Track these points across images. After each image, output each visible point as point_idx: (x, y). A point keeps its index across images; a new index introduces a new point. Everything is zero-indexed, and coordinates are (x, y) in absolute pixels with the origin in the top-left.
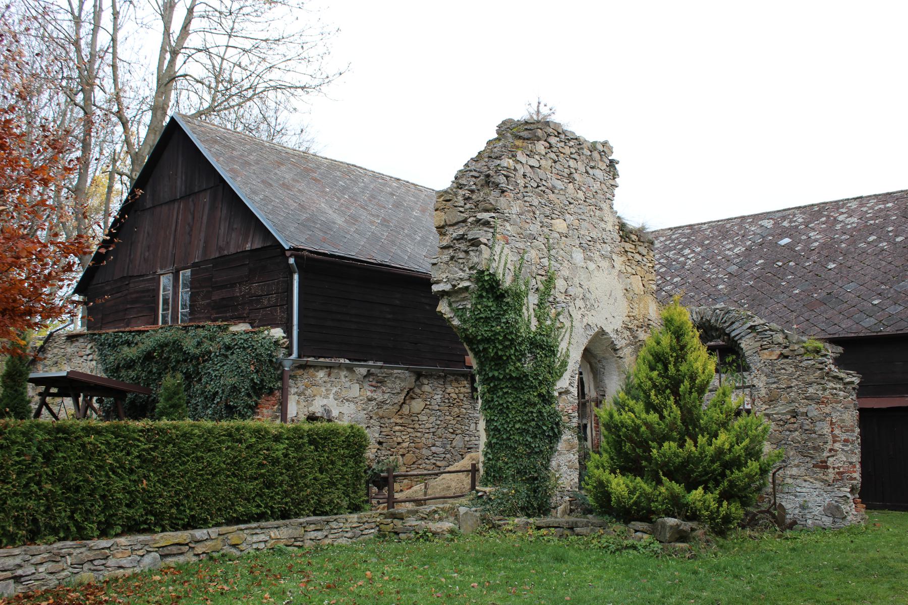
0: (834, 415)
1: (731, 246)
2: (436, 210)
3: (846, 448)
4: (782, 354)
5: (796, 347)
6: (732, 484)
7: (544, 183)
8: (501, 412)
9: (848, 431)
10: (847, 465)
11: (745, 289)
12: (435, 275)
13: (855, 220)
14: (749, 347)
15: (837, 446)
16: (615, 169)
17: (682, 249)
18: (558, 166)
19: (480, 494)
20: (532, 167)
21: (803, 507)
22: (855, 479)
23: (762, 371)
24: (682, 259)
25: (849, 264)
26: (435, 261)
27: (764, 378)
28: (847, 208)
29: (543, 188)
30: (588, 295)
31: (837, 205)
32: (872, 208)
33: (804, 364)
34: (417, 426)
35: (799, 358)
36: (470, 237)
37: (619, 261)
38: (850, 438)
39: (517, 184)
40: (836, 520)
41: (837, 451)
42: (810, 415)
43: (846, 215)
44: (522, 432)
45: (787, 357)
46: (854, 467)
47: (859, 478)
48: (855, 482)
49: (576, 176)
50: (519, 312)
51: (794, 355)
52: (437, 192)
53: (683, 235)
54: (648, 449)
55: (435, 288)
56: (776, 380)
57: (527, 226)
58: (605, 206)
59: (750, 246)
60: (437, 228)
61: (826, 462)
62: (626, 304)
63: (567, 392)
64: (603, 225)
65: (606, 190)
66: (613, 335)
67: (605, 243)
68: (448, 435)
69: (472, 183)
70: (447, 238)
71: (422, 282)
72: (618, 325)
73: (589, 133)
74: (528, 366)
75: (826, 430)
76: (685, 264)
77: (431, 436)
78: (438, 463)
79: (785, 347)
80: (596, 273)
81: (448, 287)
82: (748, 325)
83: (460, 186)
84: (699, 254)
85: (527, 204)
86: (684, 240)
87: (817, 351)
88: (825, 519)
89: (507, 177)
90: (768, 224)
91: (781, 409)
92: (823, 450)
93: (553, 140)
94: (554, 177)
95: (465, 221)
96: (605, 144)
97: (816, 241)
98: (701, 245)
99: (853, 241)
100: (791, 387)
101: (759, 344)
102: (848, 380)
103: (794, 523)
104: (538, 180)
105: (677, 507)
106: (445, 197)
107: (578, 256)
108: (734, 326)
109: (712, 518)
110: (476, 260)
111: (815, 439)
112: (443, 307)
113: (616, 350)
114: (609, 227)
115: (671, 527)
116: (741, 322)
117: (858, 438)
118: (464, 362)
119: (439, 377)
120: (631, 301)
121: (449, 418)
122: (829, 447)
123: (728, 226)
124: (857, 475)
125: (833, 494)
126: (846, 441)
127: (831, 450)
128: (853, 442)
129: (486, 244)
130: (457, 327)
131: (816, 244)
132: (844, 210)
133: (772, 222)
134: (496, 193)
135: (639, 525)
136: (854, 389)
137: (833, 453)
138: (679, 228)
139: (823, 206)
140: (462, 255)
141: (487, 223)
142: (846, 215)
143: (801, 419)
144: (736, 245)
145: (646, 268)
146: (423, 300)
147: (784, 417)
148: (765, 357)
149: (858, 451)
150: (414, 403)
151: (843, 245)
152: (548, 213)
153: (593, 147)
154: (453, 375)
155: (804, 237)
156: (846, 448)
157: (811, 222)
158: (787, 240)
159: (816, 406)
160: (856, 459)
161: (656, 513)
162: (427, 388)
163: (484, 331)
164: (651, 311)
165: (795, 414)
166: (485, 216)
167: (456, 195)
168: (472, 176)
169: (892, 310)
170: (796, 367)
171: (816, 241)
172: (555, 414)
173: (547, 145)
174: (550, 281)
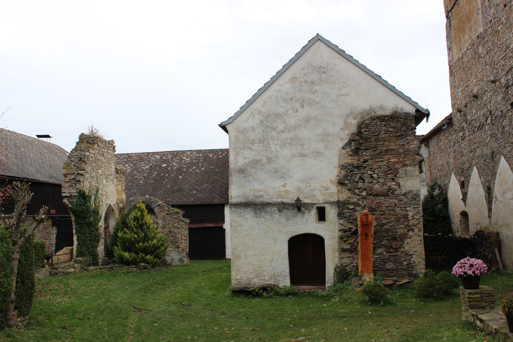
6: (157, 254)
8: (84, 234)
11: (150, 183)
13: (189, 159)
15: (183, 241)
17: (124, 164)
21: (172, 260)
25: (186, 177)
31: (183, 152)
32: (194, 155)
37: (115, 180)
44: (90, 240)
49: (105, 154)
50: (90, 202)
51: (171, 214)
54: (134, 245)
55: (63, 195)
63: (101, 226)
72: (114, 203)
73: (108, 138)
74: (92, 219)
75: (180, 237)
81: (69, 195)
84: (132, 167)
87: (177, 213)
90: (157, 156)
91: (166, 230)
95: (74, 173)
96: (112, 141)
97: (175, 166)
98: (132, 163)
99: (188, 168)
103: (170, 264)
105: (144, 260)
109: (152, 263)
112: (65, 201)
120: (118, 194)
123: (143, 156)
124: (188, 250)
130: (70, 208)
134: (83, 164)
135: (133, 266)
138: (123, 154)
139: (178, 152)
140: (74, 185)
141: (82, 175)
144: (146, 165)
155: (171, 164)
158: (164, 165)
160: (187, 245)
161: (138, 262)
163: (80, 209)
165: (170, 232)
166: (81, 172)
167: (71, 164)
169: (200, 195)
171: (175, 166)
172: (99, 234)
174: (98, 191)
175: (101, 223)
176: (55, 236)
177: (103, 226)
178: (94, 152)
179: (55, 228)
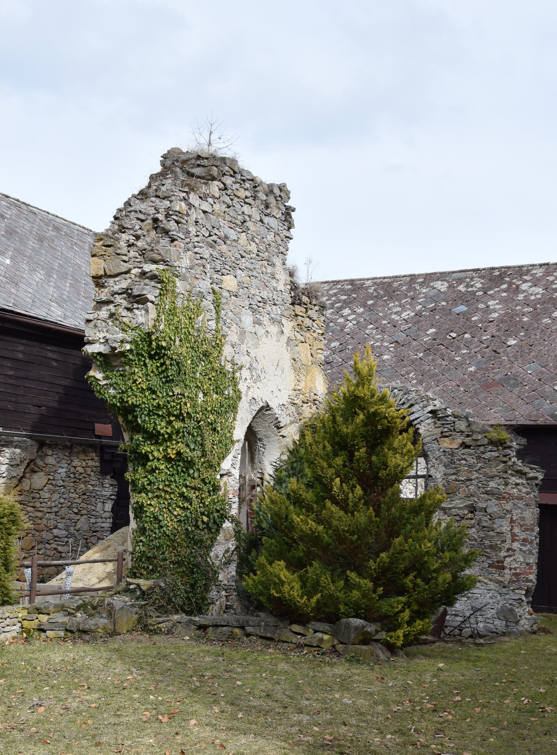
0: (515, 512)
1: (399, 309)
2: (93, 256)
3: (524, 548)
4: (463, 443)
5: (480, 437)
7: (216, 231)
9: (527, 530)
10: (524, 566)
12: (90, 333)
14: (429, 434)
15: (516, 545)
16: (291, 217)
17: (341, 309)
18: (231, 211)
19: (132, 587)
20: (205, 212)
22: (531, 581)
23: (441, 461)
24: (341, 320)
26: (91, 317)
27: (442, 468)
28: (532, 275)
29: (214, 238)
30: (254, 365)
33: (487, 455)
34: (38, 505)
35: (482, 448)
36: (136, 292)
37: (288, 326)
38: (529, 537)
39: (188, 232)
40: (509, 624)
41: (514, 551)
42: (489, 511)
43: (530, 284)
45: (468, 447)
46: (531, 568)
47: (535, 581)
48: (530, 584)
52: (96, 234)
53: (343, 291)
55: (90, 349)
56: (454, 471)
57: (196, 282)
58: (277, 261)
59: (420, 312)
60: (93, 277)
61: (503, 562)
62: (293, 376)
63: (229, 474)
64: (274, 283)
65: (280, 242)
66: (277, 411)
67: (275, 304)
68: (73, 516)
69: (137, 227)
70: (106, 290)
71: (76, 340)
72: (285, 400)
73: (267, 175)
76: (343, 327)
77: (53, 516)
78: (60, 549)
79: (468, 436)
80: (264, 339)
82: (430, 408)
83: (122, 229)
85: (198, 256)
86: (344, 297)
88: (497, 622)
89: (178, 222)
90: (441, 286)
92: (500, 549)
93: (229, 181)
94: (227, 224)
95: (128, 272)
96: (282, 188)
97: (495, 311)
98: (364, 305)
99: (536, 316)
100: (471, 480)
101: (439, 430)
102: (531, 475)
104: (210, 228)
106: (106, 242)
107: (247, 319)
108: (414, 409)
110: (141, 320)
111: (493, 537)
113: (279, 428)
114: (281, 287)
115: (356, 628)
116: (421, 405)
117: (536, 538)
118: (94, 430)
119: (65, 447)
120: (297, 371)
121: (74, 495)
122: (507, 546)
123: (396, 284)
124: (533, 577)
125: (508, 596)
126: (525, 540)
127: (508, 550)
128: (531, 543)
129: (153, 302)
131: (495, 315)
132: (527, 278)
133: (446, 284)
136: (537, 485)
137: (511, 553)
138: (338, 282)
142: (530, 284)
143: (479, 515)
144: (404, 310)
145: (315, 335)
146: (50, 355)
147: (461, 512)
148: (446, 445)
149: (535, 551)
150: (35, 477)
151: (525, 319)
152: (218, 268)
153: (270, 190)
154: (81, 445)
155: (481, 306)
156: (524, 548)
157: (490, 289)
158: (462, 308)
159: (497, 502)
160: (533, 560)
162: (50, 460)
164: (317, 385)
165: (473, 509)
168: (138, 219)
170: (479, 458)
171: (495, 311)
173: (222, 186)
175: (231, 464)
176: (109, 506)
177: (236, 473)
178: (205, 206)
179: (108, 481)
